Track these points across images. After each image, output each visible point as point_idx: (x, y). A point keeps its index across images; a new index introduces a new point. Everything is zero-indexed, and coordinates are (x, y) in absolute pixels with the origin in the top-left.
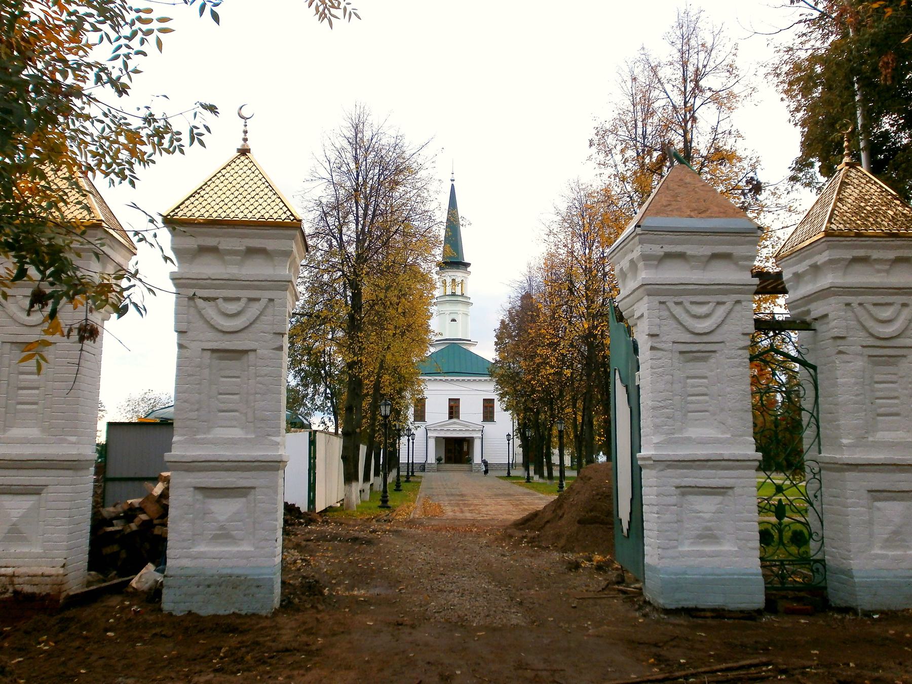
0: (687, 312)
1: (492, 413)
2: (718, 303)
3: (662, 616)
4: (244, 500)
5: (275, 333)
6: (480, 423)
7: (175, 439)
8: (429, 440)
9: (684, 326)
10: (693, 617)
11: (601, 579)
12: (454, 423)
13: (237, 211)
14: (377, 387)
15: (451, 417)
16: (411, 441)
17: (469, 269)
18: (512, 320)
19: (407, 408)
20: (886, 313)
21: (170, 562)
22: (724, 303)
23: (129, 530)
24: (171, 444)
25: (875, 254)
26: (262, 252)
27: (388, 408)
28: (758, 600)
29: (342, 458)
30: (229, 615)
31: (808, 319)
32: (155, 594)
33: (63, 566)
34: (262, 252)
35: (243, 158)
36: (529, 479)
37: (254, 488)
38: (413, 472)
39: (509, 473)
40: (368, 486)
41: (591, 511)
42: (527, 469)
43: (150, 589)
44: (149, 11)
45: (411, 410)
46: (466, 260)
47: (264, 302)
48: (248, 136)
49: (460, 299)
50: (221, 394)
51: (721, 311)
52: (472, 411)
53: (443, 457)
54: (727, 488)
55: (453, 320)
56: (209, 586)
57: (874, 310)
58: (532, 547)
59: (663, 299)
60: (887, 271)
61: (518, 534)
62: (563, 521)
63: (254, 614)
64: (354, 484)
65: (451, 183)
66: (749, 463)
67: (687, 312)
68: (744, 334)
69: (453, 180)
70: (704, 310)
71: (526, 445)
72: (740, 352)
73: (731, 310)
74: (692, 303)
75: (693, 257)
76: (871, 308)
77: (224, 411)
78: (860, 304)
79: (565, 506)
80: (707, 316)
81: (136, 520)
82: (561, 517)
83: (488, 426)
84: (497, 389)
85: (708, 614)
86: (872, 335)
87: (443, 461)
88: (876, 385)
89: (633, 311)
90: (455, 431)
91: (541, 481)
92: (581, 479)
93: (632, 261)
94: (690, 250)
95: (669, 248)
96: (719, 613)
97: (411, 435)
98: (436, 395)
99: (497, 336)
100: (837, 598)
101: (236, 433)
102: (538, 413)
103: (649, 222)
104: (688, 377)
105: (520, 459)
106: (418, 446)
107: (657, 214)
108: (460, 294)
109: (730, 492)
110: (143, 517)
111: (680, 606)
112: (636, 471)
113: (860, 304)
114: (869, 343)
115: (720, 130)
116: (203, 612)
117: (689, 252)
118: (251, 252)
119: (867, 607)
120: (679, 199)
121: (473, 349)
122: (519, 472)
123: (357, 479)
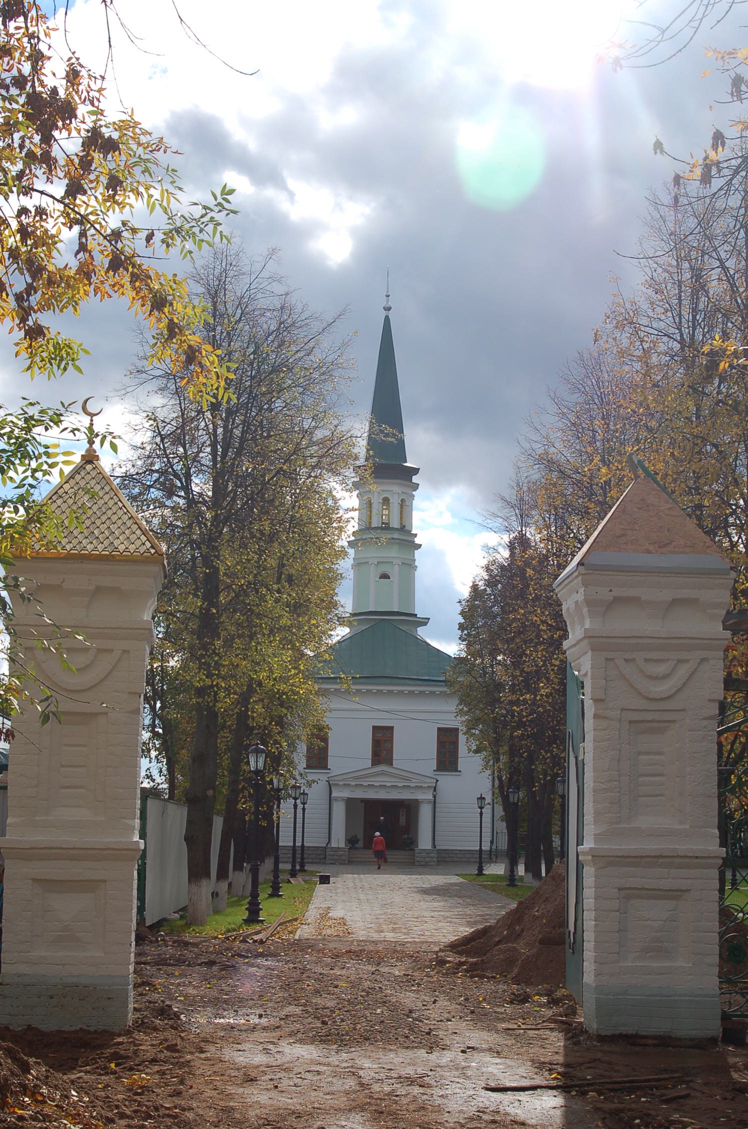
3: (595, 1043)
5: (130, 693)
7: (9, 820)
12: (383, 773)
16: (300, 806)
17: (415, 479)
18: (489, 583)
19: (292, 746)
22: (687, 661)
28: (715, 1028)
29: (185, 839)
30: (76, 1032)
37: (105, 881)
38: (302, 865)
39: (480, 869)
40: (224, 886)
42: (513, 864)
45: (302, 748)
49: (396, 536)
50: (63, 766)
51: (683, 671)
52: (415, 748)
53: (361, 836)
54: (682, 891)
55: (385, 576)
58: (471, 977)
61: (451, 958)
63: (104, 1031)
64: (204, 882)
65: (384, 313)
66: (710, 861)
68: (710, 700)
70: (661, 669)
72: (705, 723)
73: (695, 670)
74: (646, 660)
77: (67, 787)
80: (666, 677)
83: (447, 781)
85: (650, 1042)
87: (360, 844)
92: (553, 878)
95: (618, 592)
99: (462, 613)
102: (531, 759)
104: (640, 753)
105: (503, 843)
106: (310, 814)
111: (618, 1032)
112: (579, 866)
116: (43, 1028)
120: (636, 527)
123: (208, 875)
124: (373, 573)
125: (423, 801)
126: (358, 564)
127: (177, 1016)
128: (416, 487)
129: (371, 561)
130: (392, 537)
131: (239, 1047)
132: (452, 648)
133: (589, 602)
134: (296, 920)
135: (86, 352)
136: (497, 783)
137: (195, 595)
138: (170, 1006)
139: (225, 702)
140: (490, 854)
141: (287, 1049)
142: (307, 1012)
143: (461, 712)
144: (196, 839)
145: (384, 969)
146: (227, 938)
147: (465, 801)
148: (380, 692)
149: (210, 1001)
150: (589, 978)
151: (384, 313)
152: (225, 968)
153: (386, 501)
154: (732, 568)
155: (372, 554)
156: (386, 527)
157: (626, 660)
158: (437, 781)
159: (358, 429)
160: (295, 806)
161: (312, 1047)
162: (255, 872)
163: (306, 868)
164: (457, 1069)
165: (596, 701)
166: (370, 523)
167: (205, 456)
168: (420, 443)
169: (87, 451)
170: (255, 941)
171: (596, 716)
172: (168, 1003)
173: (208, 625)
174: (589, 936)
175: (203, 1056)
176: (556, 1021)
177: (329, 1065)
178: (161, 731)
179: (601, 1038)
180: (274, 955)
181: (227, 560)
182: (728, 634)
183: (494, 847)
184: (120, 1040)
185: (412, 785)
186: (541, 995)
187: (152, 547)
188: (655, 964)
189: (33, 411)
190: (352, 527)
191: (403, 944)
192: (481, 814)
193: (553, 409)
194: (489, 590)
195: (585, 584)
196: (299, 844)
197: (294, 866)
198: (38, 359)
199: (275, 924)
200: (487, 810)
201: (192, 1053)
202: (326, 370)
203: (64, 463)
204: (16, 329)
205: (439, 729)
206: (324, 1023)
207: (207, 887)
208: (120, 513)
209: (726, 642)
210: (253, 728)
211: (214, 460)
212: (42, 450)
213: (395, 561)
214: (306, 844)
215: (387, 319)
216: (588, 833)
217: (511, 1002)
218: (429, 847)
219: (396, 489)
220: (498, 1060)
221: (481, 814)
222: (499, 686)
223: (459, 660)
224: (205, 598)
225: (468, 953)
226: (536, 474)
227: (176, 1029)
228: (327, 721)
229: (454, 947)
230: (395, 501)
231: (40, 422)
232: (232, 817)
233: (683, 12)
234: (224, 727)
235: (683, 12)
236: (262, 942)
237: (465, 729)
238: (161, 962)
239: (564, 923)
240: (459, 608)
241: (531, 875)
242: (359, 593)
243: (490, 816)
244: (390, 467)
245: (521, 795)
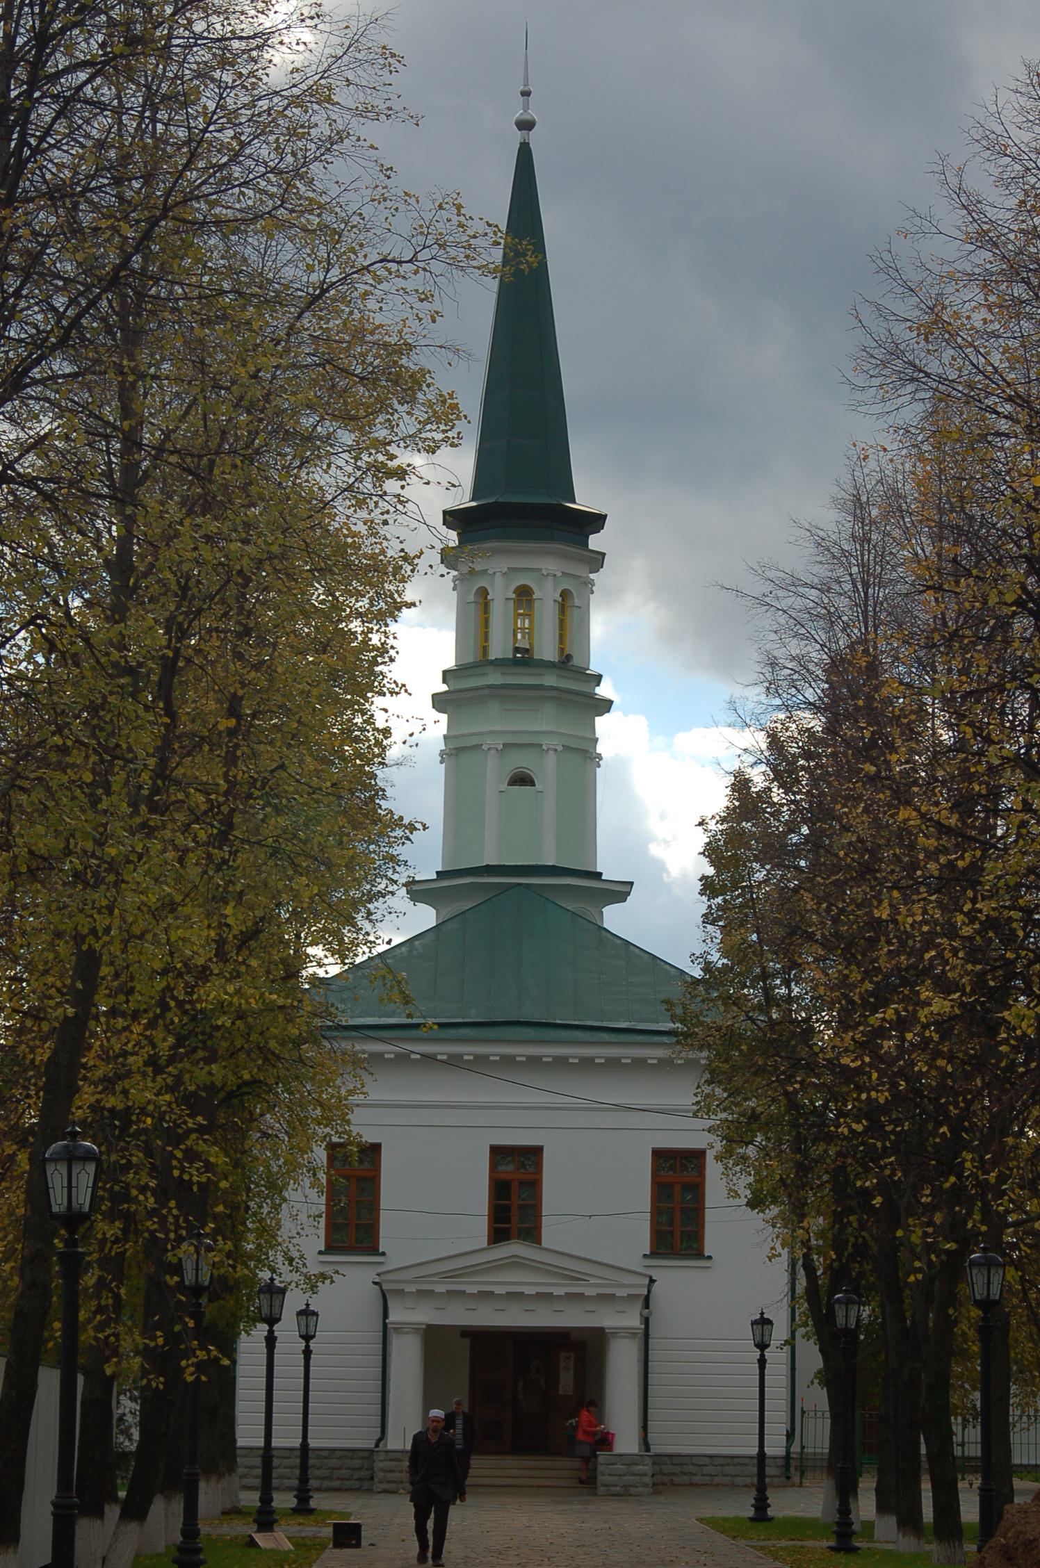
8: (396, 1342)
12: (515, 1263)
15: (498, 1234)
17: (595, 542)
27: (85, 1176)
36: (844, 1535)
39: (761, 1505)
42: (846, 1491)
49: (550, 680)
55: (522, 780)
65: (517, 136)
69: (526, 94)
71: (841, 1378)
83: (675, 1281)
84: (703, 1108)
90: (517, 1298)
91: (907, 1544)
98: (430, 1140)
99: (712, 852)
102: (893, 1216)
105: (818, 1437)
121: (614, 918)
122: (807, 1502)
124: (494, 772)
125: (617, 1332)
128: (597, 561)
129: (488, 742)
136: (802, 1282)
140: (787, 1467)
143: (703, 1108)
151: (517, 136)
153: (524, 595)
155: (496, 723)
156: (523, 659)
158: (652, 1281)
163: (313, 1504)
166: (485, 650)
183: (795, 1448)
185: (589, 1292)
192: (762, 1362)
194: (777, 795)
200: (777, 1358)
205: (658, 1154)
213: (547, 742)
214: (312, 1443)
219: (550, 565)
221: (762, 1362)
230: (547, 596)
233: (793, 1369)
235: (793, 1369)
237: (719, 1146)
241: (892, 1520)
243: (784, 1369)
244: (527, 512)
245: (866, 1312)
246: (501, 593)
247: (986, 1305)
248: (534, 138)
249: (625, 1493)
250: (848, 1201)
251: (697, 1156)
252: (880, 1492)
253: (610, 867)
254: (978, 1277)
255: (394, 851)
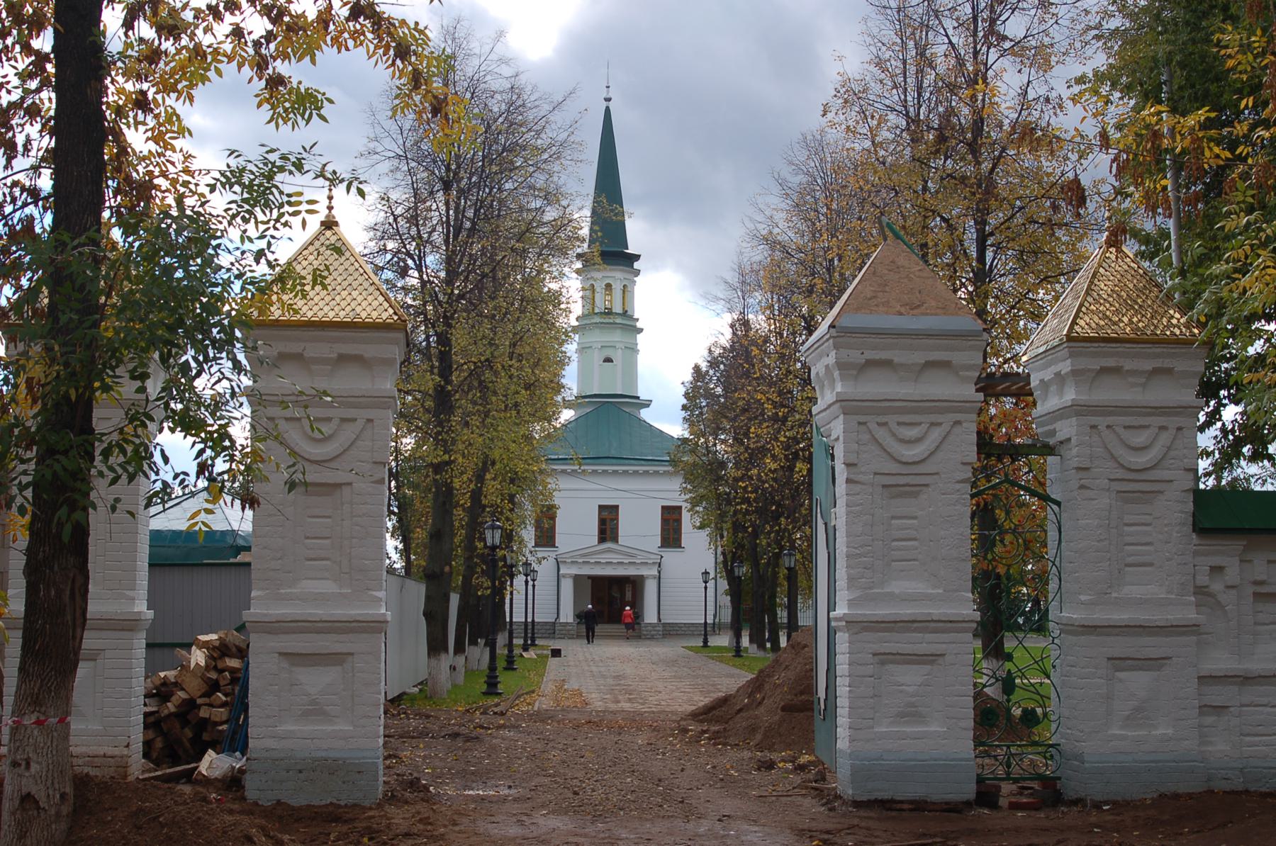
0: (894, 435)
1: (678, 531)
2: (932, 424)
4: (339, 668)
5: (375, 463)
6: (655, 550)
7: (253, 594)
9: (889, 453)
10: (888, 810)
11: (796, 779)
13: (326, 309)
14: (476, 495)
15: (602, 540)
16: (531, 583)
17: (636, 265)
18: (713, 363)
20: (1140, 439)
21: (251, 743)
22: (940, 424)
23: (166, 712)
24: (250, 599)
25: (1128, 365)
26: (358, 359)
27: (498, 534)
31: (1052, 442)
32: (233, 782)
33: (127, 746)
34: (358, 359)
35: (328, 233)
36: (738, 651)
37: (352, 654)
38: (533, 640)
39: (705, 641)
40: (461, 660)
41: (802, 693)
42: (738, 636)
43: (225, 777)
44: (301, 194)
46: (631, 250)
47: (360, 424)
48: (334, 203)
49: (618, 320)
51: (936, 434)
52: (639, 528)
55: (608, 360)
56: (300, 772)
57: (1125, 434)
58: (715, 744)
59: (862, 419)
60: (1144, 386)
62: (762, 709)
63: (355, 805)
64: (443, 656)
65: (605, 104)
66: (964, 625)
67: (894, 435)
72: (958, 486)
73: (949, 432)
74: (899, 424)
75: (902, 365)
76: (1121, 431)
78: (1108, 427)
79: (767, 687)
80: (919, 440)
81: (173, 699)
82: (760, 703)
83: (670, 556)
85: (905, 806)
86: (1122, 466)
88: (1126, 528)
89: (830, 430)
90: (610, 564)
91: (761, 654)
92: (793, 647)
93: (827, 366)
94: (897, 356)
95: (870, 355)
96: (919, 806)
97: (530, 572)
98: (576, 503)
99: (686, 395)
100: (1071, 789)
101: (329, 587)
102: (755, 535)
103: (846, 322)
104: (893, 518)
105: (727, 616)
106: (542, 591)
107: (858, 309)
108: (619, 310)
109: (940, 660)
110: (182, 694)
111: (873, 798)
112: (831, 633)
113: (1108, 427)
114: (1118, 476)
115: (1031, 95)
116: (294, 802)
117: (896, 360)
118: (343, 359)
119: (1098, 798)
120: (887, 289)
121: (645, 414)
122: (722, 640)
123: (446, 650)
124: (597, 357)
125: (648, 577)
126: (582, 350)
127: (426, 788)
128: (637, 273)
129: (595, 345)
130: (616, 322)
131: (493, 819)
132: (676, 428)
133: (840, 365)
134: (533, 692)
135: (331, 101)
137: (432, 373)
138: (418, 779)
139: (462, 484)
141: (541, 821)
142: (556, 782)
144: (434, 615)
145: (626, 738)
146: (468, 711)
147: (689, 578)
148: (605, 472)
149: (458, 772)
150: (843, 744)
151: (605, 104)
152: (468, 739)
153: (609, 286)
154: (984, 330)
155: (597, 338)
156: (609, 312)
157: (879, 424)
159: (582, 217)
160: (527, 582)
161: (566, 818)
162: (492, 645)
164: (716, 838)
165: (848, 465)
167: (437, 238)
168: (637, 235)
169: (327, 216)
170: (495, 713)
171: (848, 481)
172: (415, 775)
173: (443, 401)
174: (843, 702)
175: (457, 828)
176: (807, 788)
177: (586, 836)
178: (396, 510)
179: (857, 804)
180: (515, 727)
181: (460, 338)
182: (981, 396)
184: (371, 813)
186: (785, 762)
187: (395, 313)
188: (908, 729)
189: (273, 157)
190: (577, 309)
191: (641, 714)
193: (776, 190)
195: (836, 347)
196: (530, 620)
197: (526, 641)
198: (281, 110)
199: (512, 697)
200: (711, 584)
201: (445, 826)
202: (558, 151)
203: (308, 212)
204: (256, 79)
206: (576, 793)
207: (447, 660)
208: (361, 279)
209: (979, 405)
210: (485, 507)
211: (447, 242)
212: (285, 199)
213: (618, 345)
215: (608, 110)
216: (836, 597)
217: (759, 769)
218: (656, 621)
220: (756, 829)
222: (722, 465)
223: (684, 441)
224: (441, 375)
225: (710, 721)
226: (760, 254)
227: (427, 801)
228: (557, 500)
229: (697, 716)
230: (617, 287)
231: (282, 169)
232: (467, 590)
234: (457, 505)
236: (502, 714)
238: (405, 736)
239: (810, 689)
240: (683, 390)
242: (583, 375)
244: (613, 253)
246: (600, 287)
247: (789, 569)
248: (611, 104)
249: (652, 638)
250: (737, 527)
251: (678, 509)
252: (751, 636)
253: (643, 394)
254: (786, 559)
255: (372, 233)
